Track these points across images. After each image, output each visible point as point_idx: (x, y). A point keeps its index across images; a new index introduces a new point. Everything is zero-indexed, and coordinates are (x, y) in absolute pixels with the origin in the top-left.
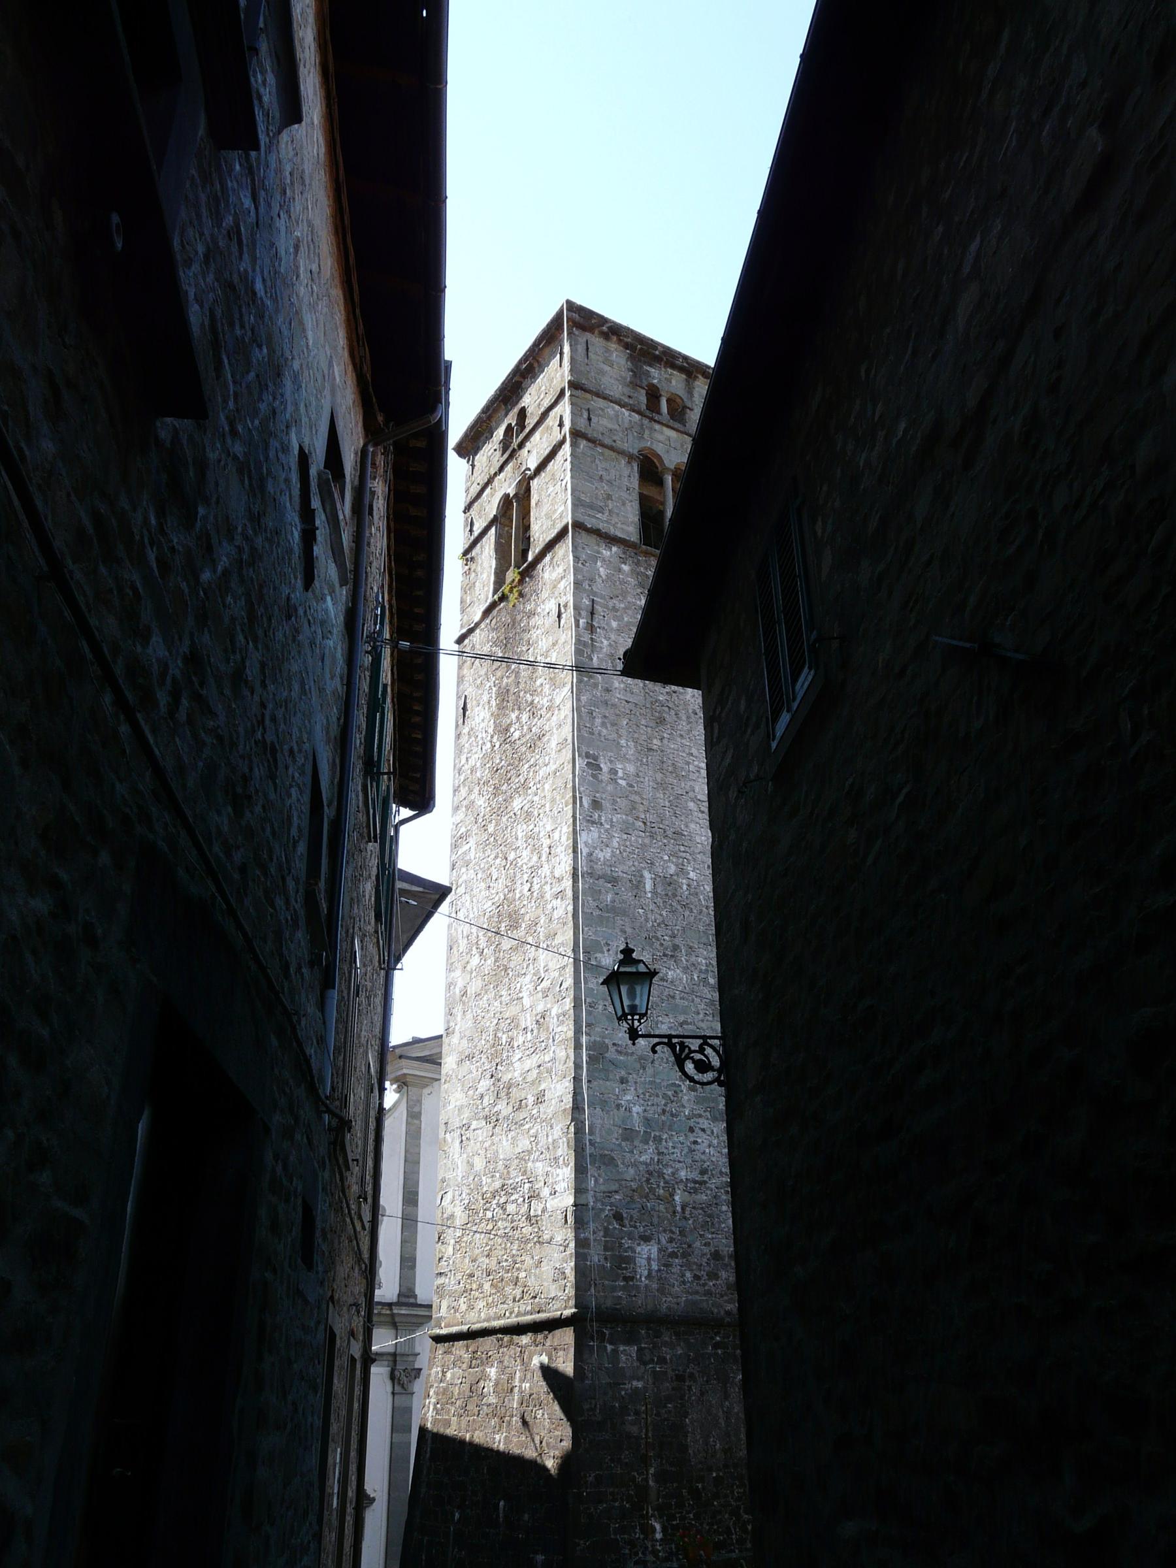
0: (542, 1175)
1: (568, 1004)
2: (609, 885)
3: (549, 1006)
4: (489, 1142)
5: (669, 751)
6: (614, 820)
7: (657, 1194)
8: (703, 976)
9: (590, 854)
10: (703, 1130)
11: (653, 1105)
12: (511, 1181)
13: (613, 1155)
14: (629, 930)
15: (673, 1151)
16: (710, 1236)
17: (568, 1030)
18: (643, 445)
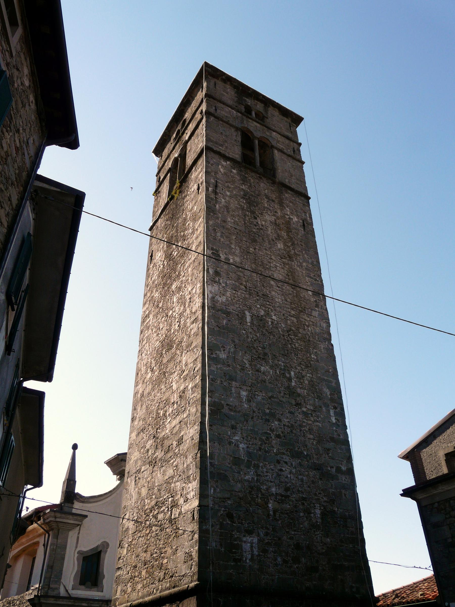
0: (180, 490)
1: (198, 379)
2: (225, 315)
3: (187, 385)
4: (150, 477)
5: (259, 255)
6: (228, 283)
7: (256, 502)
8: (282, 372)
9: (213, 298)
10: (286, 463)
11: (253, 444)
12: (161, 499)
13: (226, 473)
14: (237, 341)
15: (266, 474)
16: (293, 533)
17: (198, 395)
18: (242, 125)
